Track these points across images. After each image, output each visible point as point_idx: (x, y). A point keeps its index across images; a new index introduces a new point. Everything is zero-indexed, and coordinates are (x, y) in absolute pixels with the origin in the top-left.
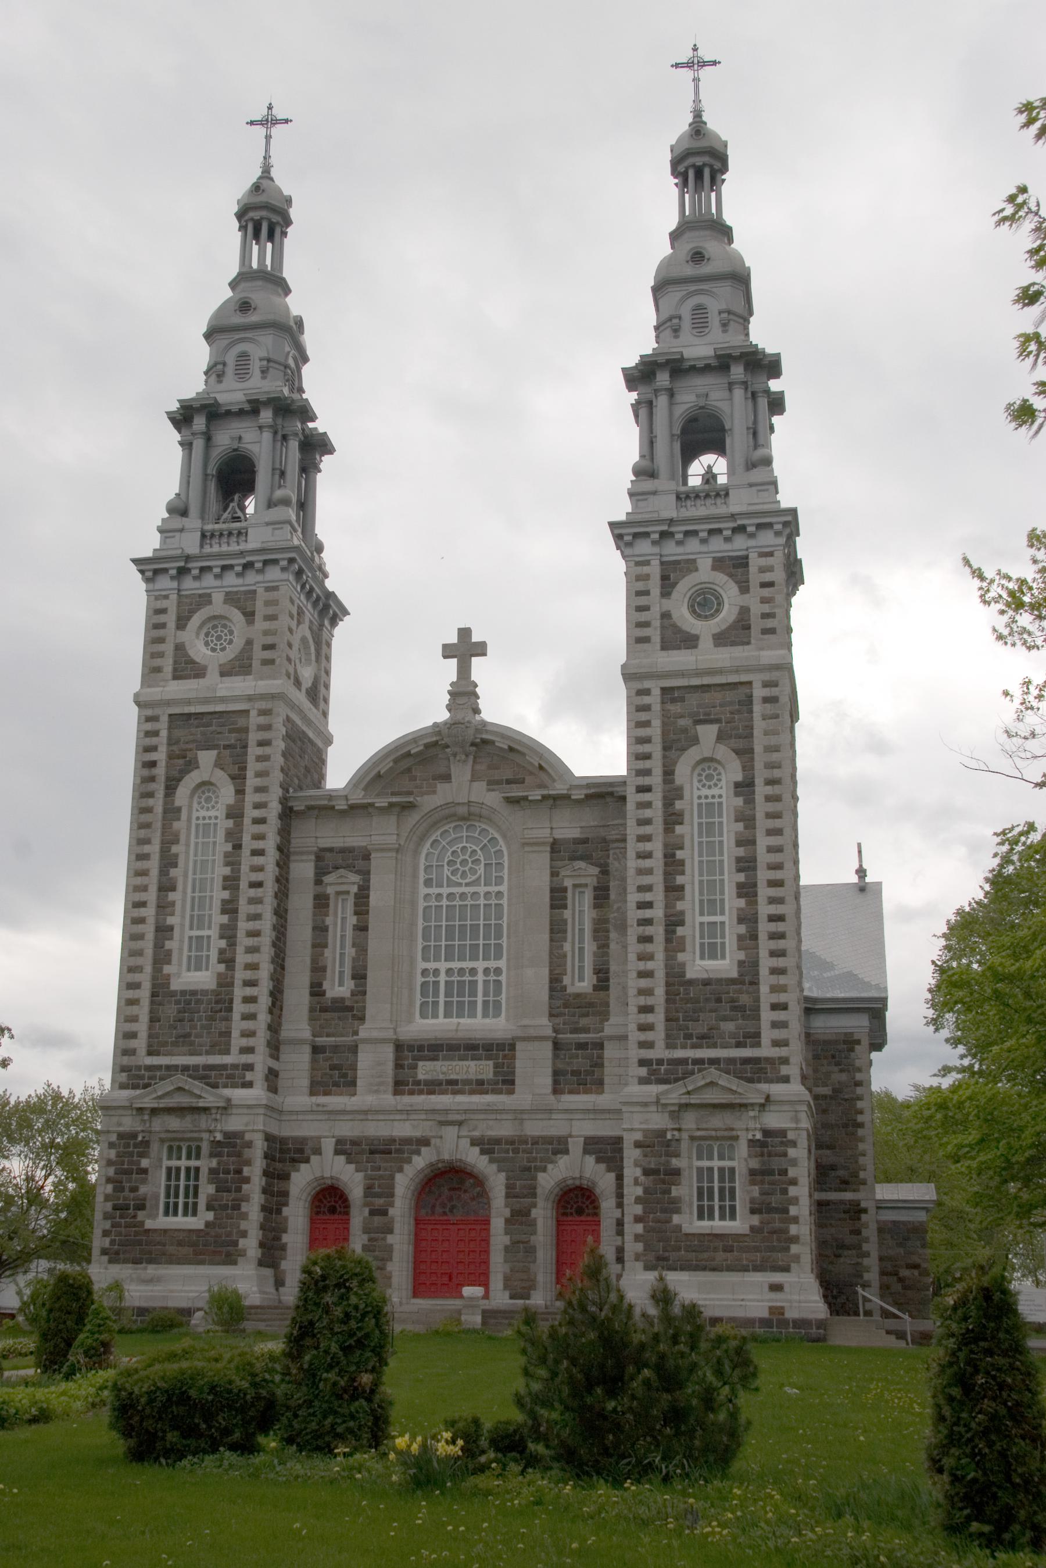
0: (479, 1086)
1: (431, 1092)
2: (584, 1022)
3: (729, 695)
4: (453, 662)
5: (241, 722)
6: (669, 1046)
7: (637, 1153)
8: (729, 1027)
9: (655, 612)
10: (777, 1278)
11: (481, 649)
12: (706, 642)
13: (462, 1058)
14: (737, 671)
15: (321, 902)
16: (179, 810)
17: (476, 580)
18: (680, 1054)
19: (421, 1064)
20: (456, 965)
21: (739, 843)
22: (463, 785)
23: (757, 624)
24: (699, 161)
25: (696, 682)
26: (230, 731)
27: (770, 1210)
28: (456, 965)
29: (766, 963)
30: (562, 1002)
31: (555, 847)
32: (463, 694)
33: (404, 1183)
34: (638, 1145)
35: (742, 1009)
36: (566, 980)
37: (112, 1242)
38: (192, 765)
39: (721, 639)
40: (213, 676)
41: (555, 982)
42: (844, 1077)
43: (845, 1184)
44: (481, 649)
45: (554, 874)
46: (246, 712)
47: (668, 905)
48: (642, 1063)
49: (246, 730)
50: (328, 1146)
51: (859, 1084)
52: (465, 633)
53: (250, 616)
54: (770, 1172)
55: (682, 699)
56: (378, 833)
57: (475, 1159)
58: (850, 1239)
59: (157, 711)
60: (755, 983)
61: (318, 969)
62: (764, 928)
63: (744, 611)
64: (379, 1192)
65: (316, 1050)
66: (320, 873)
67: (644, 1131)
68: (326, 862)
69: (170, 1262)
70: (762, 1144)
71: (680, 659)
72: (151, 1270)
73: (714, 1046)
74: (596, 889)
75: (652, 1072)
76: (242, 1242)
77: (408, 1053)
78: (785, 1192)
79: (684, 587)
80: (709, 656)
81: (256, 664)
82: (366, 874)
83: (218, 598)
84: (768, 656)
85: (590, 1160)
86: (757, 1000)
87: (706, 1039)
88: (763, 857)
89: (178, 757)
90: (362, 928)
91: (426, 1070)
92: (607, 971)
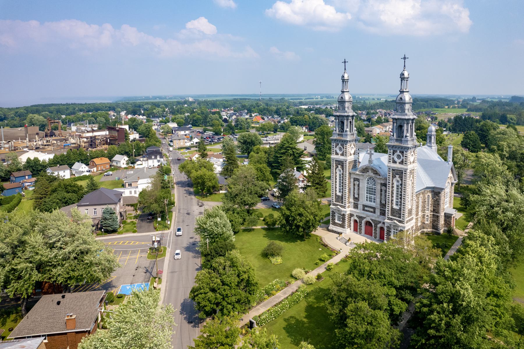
0: (372, 212)
15: (354, 184)
23: (404, 162)
29: (402, 209)
31: (381, 184)
33: (363, 222)
38: (338, 167)
39: (400, 163)
40: (339, 155)
41: (381, 201)
43: (436, 213)
50: (355, 215)
57: (370, 221)
61: (354, 193)
64: (361, 223)
66: (354, 181)
68: (355, 180)
77: (364, 206)
79: (396, 154)
80: (397, 166)
84: (405, 167)
88: (403, 195)
91: (366, 208)
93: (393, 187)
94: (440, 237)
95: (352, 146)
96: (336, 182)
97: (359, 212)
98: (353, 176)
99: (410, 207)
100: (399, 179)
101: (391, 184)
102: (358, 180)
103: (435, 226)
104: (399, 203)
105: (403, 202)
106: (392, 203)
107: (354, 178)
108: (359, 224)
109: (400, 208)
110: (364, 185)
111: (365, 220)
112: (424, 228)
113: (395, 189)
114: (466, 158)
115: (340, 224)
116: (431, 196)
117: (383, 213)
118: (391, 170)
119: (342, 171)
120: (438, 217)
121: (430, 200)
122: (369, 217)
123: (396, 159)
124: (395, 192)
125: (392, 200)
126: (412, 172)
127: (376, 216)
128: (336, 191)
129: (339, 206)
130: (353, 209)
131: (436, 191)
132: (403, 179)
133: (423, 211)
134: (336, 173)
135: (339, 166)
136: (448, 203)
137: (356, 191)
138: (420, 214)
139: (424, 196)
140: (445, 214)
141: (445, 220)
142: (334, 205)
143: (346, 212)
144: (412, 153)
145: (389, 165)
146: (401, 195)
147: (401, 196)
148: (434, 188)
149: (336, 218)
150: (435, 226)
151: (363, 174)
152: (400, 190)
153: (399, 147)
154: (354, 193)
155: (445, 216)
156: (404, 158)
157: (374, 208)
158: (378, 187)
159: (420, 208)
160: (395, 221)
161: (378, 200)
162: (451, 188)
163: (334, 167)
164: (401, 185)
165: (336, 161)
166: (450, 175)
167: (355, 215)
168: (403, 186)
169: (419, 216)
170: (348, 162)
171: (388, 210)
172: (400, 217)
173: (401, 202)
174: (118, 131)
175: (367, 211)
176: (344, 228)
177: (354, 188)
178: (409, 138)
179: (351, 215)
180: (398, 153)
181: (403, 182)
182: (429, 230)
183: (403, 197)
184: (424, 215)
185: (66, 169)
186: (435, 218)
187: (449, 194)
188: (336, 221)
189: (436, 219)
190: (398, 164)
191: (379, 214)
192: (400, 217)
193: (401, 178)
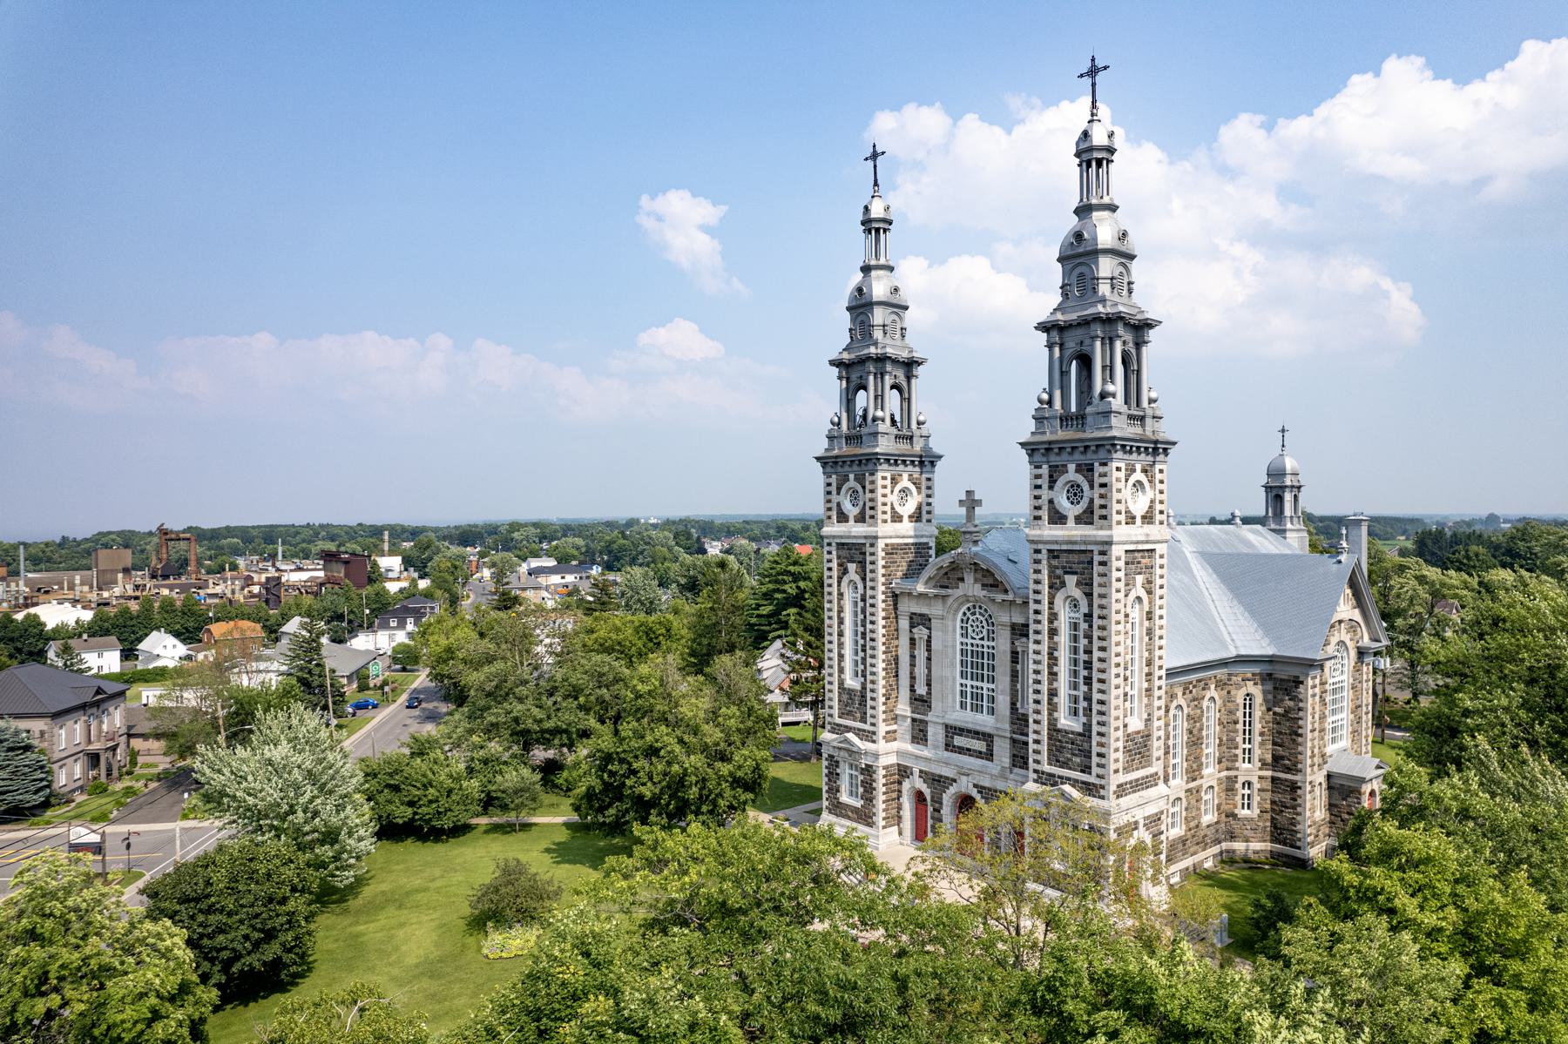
0: (979, 755)
3: (1083, 558)
8: (1078, 760)
9: (1045, 498)
14: (1085, 543)
15: (913, 641)
20: (975, 683)
21: (1086, 652)
23: (1098, 512)
25: (1064, 547)
29: (1095, 728)
33: (948, 798)
39: (1079, 520)
42: (1291, 703)
43: (1288, 770)
47: (1050, 683)
48: (1035, 771)
50: (916, 771)
51: (1300, 709)
57: (974, 793)
58: (1289, 802)
61: (913, 678)
62: (1095, 707)
64: (938, 801)
65: (914, 720)
66: (912, 626)
71: (1057, 532)
77: (952, 730)
80: (1071, 531)
84: (1103, 533)
88: (1096, 665)
90: (929, 659)
91: (959, 741)
93: (1053, 632)
94: (1307, 875)
95: (905, 482)
96: (841, 634)
97: (931, 756)
98: (907, 607)
99: (1135, 724)
100: (1077, 593)
101: (1044, 618)
103: (1283, 829)
104: (1083, 704)
105: (1096, 696)
106: (1053, 707)
107: (912, 616)
108: (930, 809)
109: (1088, 727)
110: (950, 637)
111: (952, 790)
112: (1232, 837)
113: (1063, 639)
114: (1437, 595)
115: (855, 810)
116: (1259, 699)
117: (1020, 760)
118: (1044, 556)
119: (860, 586)
120: (1294, 787)
121: (1258, 714)
122: (969, 774)
123: (1063, 503)
124: (1063, 656)
125: (1053, 693)
126: (1140, 559)
127: (990, 772)
128: (841, 670)
129: (850, 736)
130: (910, 747)
131: (1284, 673)
132: (1096, 591)
133: (1227, 760)
134: (841, 595)
135: (852, 567)
136: (1345, 732)
137: (921, 671)
138: (1211, 773)
139: (1229, 698)
140: (1329, 776)
141: (1331, 806)
142: (836, 729)
143: (876, 756)
144: (1138, 475)
145: (1034, 533)
146: (1088, 665)
147: (1089, 672)
148: (1271, 660)
149: (844, 784)
150: (1283, 829)
151: (943, 592)
152: (1083, 642)
153: (1070, 447)
154: (913, 678)
155: (1330, 788)
156: (1098, 491)
157: (988, 738)
158: (1003, 643)
159: (1210, 750)
160: (1067, 788)
161: (1003, 702)
162: (1357, 670)
163: (835, 574)
164: (1088, 617)
165: (840, 546)
166: (1346, 609)
167: (916, 771)
168: (1096, 622)
169: (1205, 783)
170: (881, 544)
171: (1038, 735)
172: (1086, 769)
173: (1088, 698)
174: (346, 562)
176: (870, 825)
177: (913, 657)
178: (1117, 403)
179: (903, 772)
180: (1072, 474)
181: (1096, 601)
182: (1256, 846)
183: (1096, 675)
184: (1232, 781)
185: (110, 647)
186: (1285, 793)
187: (1347, 694)
188: (844, 798)
189: (1286, 799)
190: (1071, 523)
191: (1007, 761)
192: (1086, 769)
193: (1086, 585)
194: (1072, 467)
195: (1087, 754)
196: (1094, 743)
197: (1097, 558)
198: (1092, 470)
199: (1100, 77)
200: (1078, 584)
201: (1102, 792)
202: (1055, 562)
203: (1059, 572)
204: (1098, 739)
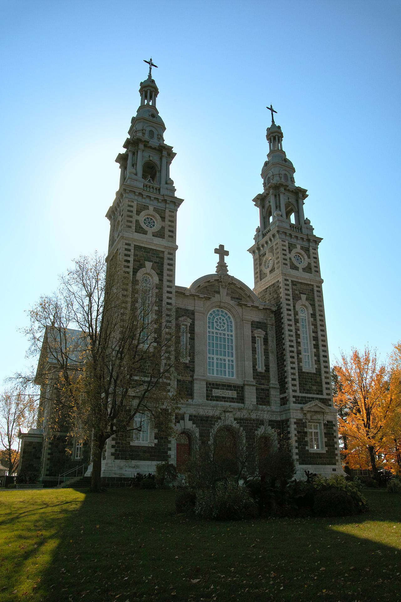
0: (232, 400)
1: (217, 401)
2: (263, 381)
4: (218, 255)
5: (161, 255)
6: (300, 392)
7: (295, 426)
8: (314, 388)
10: (334, 467)
11: (227, 253)
12: (301, 270)
13: (227, 389)
14: (311, 280)
16: (138, 281)
17: (213, 233)
18: (304, 395)
19: (213, 390)
20: (219, 357)
21: (313, 332)
22: (224, 297)
24: (274, 135)
26: (157, 257)
27: (330, 446)
28: (219, 357)
30: (256, 375)
31: (253, 323)
32: (222, 266)
34: (295, 423)
35: (317, 382)
36: (257, 367)
37: (116, 450)
38: (142, 266)
40: (150, 236)
41: (254, 366)
44: (227, 253)
45: (252, 332)
46: (163, 252)
48: (294, 397)
49: (163, 258)
52: (222, 247)
53: (163, 219)
54: (329, 434)
55: (296, 285)
56: (198, 306)
57: (235, 425)
59: (130, 242)
60: (320, 375)
63: (309, 264)
67: (297, 419)
69: (141, 459)
70: (327, 425)
71: (293, 272)
72: (134, 463)
73: (311, 393)
74: (264, 339)
75: (296, 400)
76: (169, 452)
77: (211, 386)
78: (333, 440)
79: (294, 251)
81: (166, 236)
82: (193, 320)
83: (151, 208)
85: (270, 427)
86: (321, 380)
87: (309, 392)
89: (137, 261)
91: (216, 392)
92: (269, 366)
102: (191, 314)
172: (320, 392)
175: (218, 399)
194: (299, 247)
195: (320, 384)
196: (323, 377)
197: (316, 289)
198: (309, 251)
199: (270, 111)
200: (307, 299)
201: (330, 403)
202: (295, 287)
203: (297, 292)
204: (325, 375)
